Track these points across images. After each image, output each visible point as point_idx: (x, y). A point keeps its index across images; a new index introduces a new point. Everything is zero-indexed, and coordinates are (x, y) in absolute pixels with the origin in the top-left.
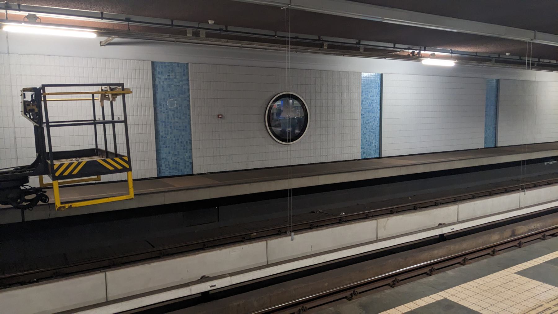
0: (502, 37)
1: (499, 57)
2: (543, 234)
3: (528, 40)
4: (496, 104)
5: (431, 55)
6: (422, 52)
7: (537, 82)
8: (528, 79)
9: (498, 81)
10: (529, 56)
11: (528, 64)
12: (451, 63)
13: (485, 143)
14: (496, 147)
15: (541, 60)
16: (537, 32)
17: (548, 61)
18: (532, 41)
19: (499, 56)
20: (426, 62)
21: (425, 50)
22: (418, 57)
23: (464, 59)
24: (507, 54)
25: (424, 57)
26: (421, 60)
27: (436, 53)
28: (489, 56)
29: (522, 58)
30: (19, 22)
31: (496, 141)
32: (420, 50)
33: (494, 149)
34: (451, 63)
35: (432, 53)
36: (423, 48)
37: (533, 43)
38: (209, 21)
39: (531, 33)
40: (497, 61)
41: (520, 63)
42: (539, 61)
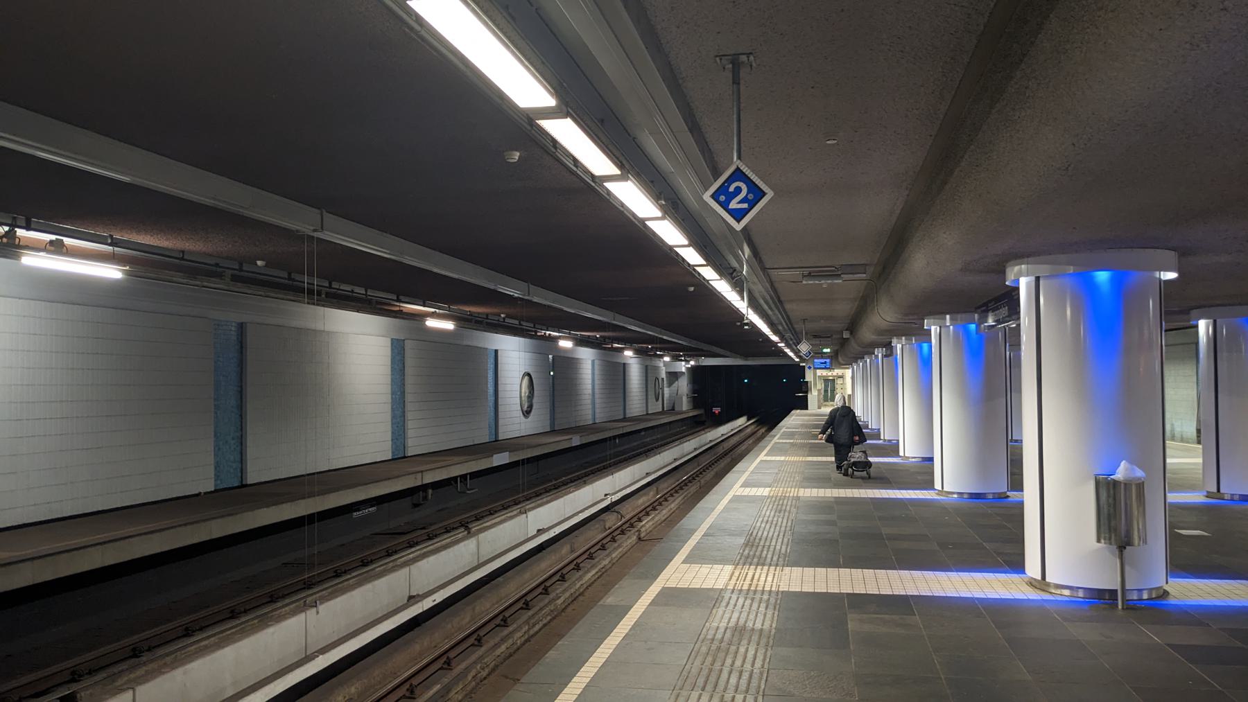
0: (247, 213)
1: (241, 270)
2: (501, 617)
3: (306, 229)
4: (246, 381)
5: (51, 242)
6: (20, 232)
7: (328, 333)
8: (312, 326)
9: (241, 327)
10: (311, 274)
11: (311, 292)
12: (112, 273)
13: (217, 477)
14: (243, 486)
15: (335, 285)
16: (327, 216)
17: (348, 288)
18: (316, 235)
19: (241, 264)
20: (31, 260)
21: (28, 228)
22: (7, 245)
23: (145, 265)
24: (259, 263)
25: (27, 247)
26: (17, 257)
27: (68, 241)
28: (217, 265)
29: (293, 276)
30: (38, 250)
31: (243, 471)
32: (13, 226)
33: (237, 494)
34: (112, 273)
35: (53, 237)
36: (22, 222)
37: (318, 239)
38: (259, 263)
39: (313, 213)
40: (235, 279)
41: (294, 290)
42: (330, 287)
